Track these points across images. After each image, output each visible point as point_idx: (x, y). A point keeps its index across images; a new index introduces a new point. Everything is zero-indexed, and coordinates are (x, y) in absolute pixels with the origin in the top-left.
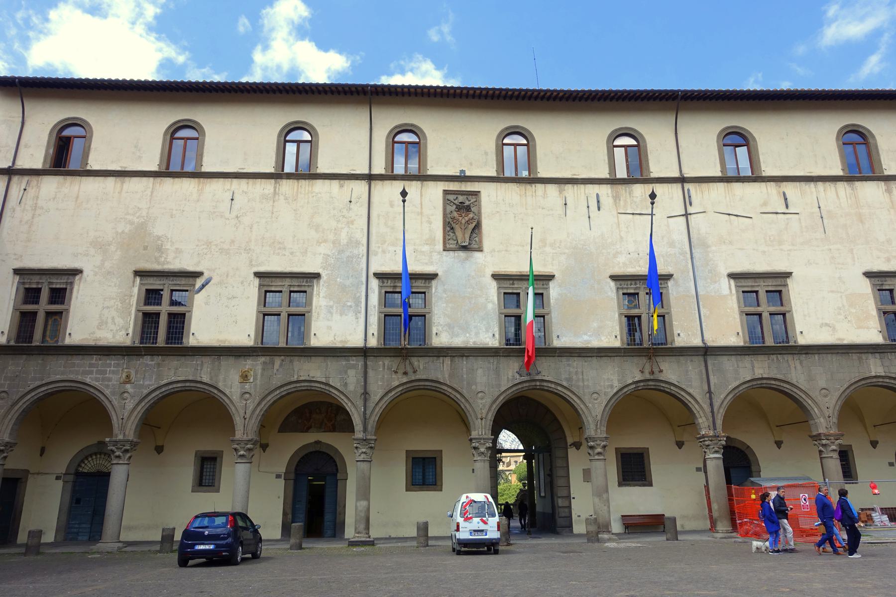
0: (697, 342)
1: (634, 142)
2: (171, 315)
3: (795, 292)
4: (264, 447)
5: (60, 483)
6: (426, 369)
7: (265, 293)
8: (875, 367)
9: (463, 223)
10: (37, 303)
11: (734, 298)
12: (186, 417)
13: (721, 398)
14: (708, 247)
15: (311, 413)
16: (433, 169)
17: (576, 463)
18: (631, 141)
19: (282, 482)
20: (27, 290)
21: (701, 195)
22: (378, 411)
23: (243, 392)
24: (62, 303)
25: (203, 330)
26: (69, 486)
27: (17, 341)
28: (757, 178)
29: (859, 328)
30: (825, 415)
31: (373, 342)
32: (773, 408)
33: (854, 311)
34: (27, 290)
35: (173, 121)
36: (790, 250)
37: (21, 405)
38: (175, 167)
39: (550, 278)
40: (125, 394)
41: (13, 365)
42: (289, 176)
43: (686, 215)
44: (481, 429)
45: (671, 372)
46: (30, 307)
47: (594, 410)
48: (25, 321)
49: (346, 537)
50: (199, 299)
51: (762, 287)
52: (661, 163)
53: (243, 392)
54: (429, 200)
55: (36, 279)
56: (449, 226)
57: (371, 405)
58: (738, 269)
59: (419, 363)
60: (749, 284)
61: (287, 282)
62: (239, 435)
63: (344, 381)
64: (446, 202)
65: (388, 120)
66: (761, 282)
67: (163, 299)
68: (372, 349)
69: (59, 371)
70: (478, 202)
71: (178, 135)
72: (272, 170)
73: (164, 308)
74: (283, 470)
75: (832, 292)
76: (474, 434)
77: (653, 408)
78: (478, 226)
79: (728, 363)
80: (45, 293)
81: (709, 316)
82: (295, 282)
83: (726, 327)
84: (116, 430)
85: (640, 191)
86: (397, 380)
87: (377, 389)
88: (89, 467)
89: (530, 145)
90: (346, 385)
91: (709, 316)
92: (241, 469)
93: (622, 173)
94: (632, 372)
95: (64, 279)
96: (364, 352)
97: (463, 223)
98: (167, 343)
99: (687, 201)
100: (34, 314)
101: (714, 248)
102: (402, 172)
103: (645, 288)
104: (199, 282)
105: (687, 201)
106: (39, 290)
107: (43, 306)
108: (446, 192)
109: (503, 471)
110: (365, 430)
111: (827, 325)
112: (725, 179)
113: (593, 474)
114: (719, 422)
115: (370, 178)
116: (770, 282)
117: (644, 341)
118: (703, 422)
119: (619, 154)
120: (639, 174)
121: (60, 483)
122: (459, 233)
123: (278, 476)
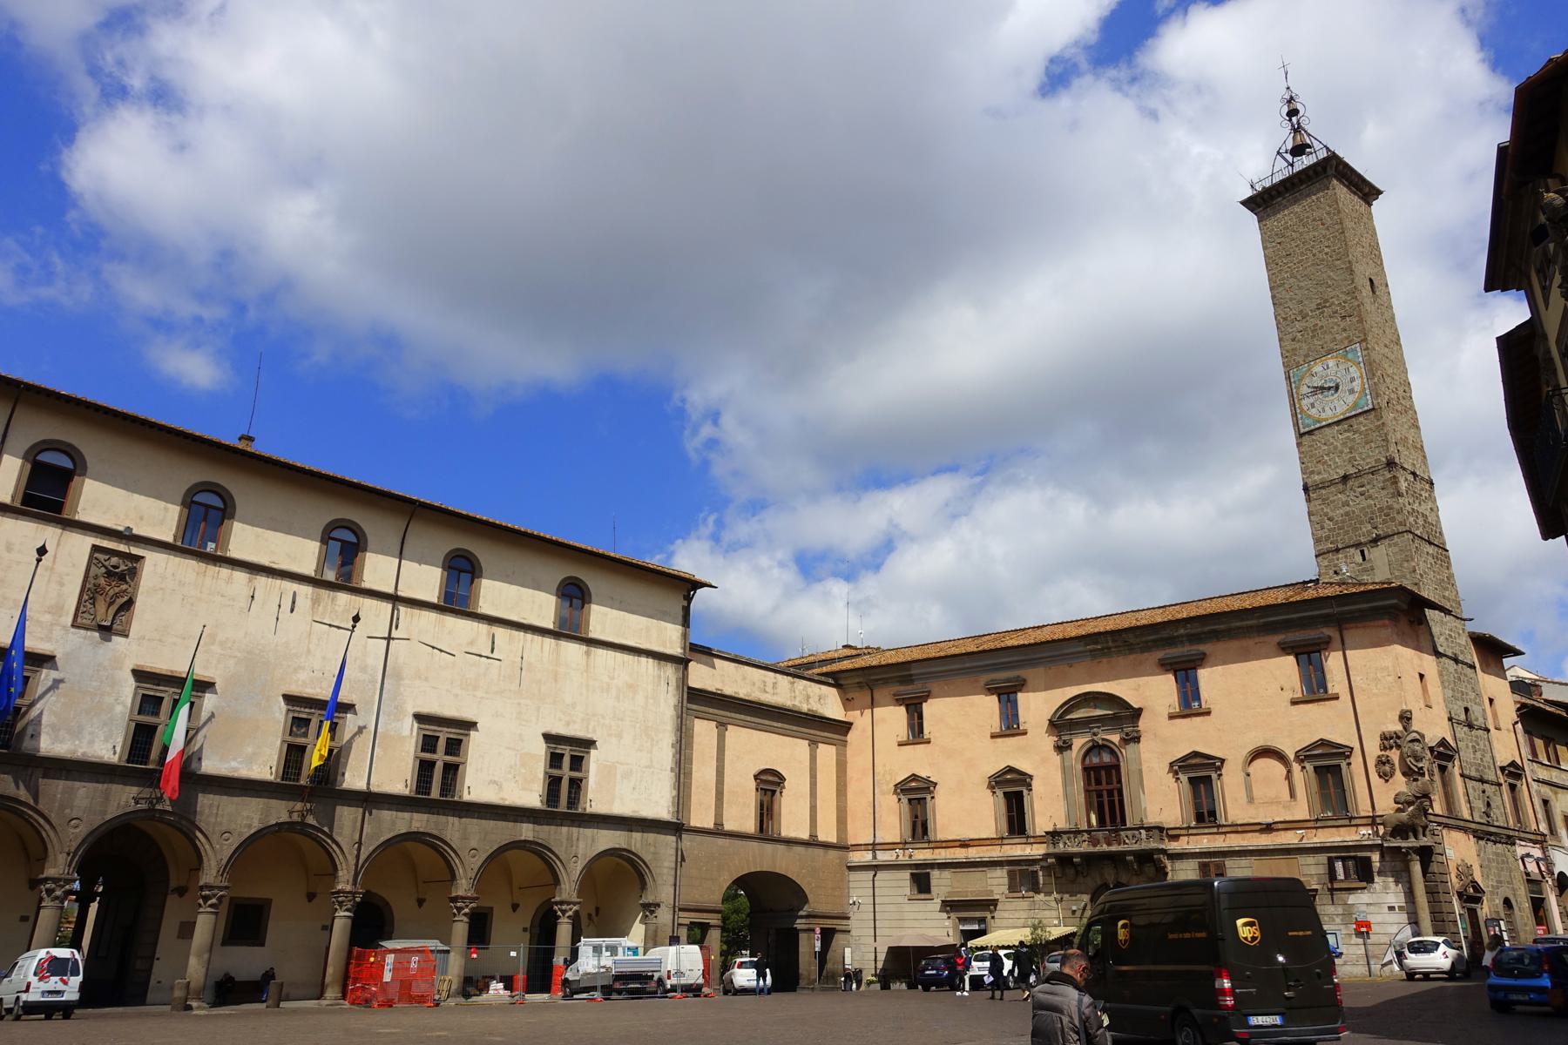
8: (527, 831)
10: (434, 752)
29: (524, 789)
43: (389, 638)
51: (444, 734)
56: (90, 593)
58: (426, 709)
83: (396, 776)
99: (394, 623)
100: (432, 764)
105: (394, 623)
111: (495, 782)
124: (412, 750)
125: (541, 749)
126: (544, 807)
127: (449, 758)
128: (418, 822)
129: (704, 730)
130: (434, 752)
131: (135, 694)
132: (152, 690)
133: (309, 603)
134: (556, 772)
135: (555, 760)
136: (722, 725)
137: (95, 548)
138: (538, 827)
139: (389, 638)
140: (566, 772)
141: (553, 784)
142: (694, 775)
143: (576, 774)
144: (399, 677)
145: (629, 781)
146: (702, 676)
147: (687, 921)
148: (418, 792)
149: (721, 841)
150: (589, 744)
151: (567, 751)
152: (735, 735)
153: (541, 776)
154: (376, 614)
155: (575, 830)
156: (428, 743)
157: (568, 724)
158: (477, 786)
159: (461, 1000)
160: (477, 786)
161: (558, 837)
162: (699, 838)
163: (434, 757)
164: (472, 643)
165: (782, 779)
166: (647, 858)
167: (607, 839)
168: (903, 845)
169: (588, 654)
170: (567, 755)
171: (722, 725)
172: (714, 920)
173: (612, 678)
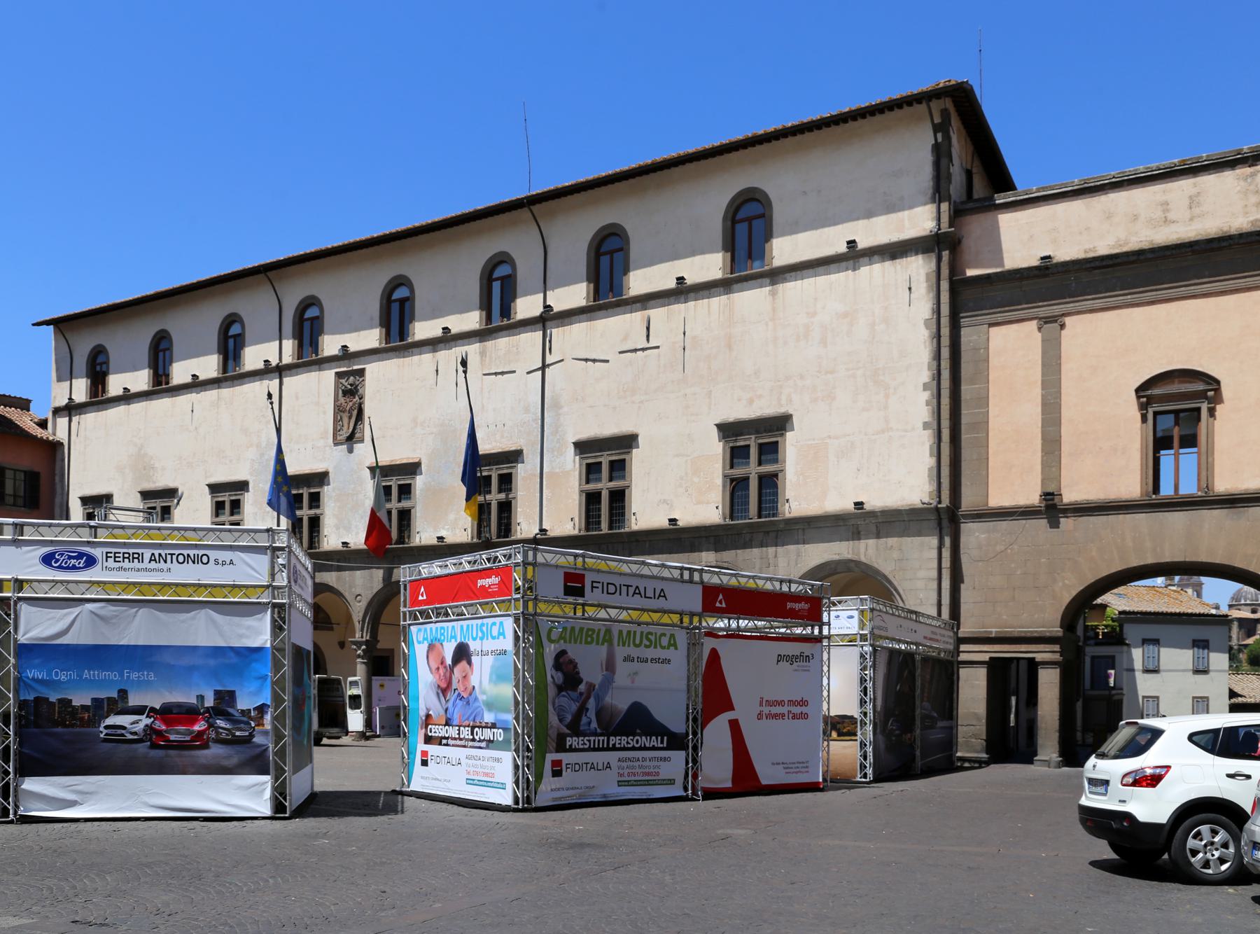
9: (350, 418)
11: (577, 473)
14: (561, 407)
21: (566, 338)
29: (699, 503)
33: (696, 480)
36: (642, 402)
39: (412, 469)
43: (544, 367)
46: (768, 468)
49: (350, 729)
51: (605, 459)
71: (740, 215)
75: (677, 456)
83: (565, 518)
97: (350, 418)
98: (732, 518)
99: (546, 347)
100: (745, 480)
101: (565, 409)
105: (546, 347)
111: (665, 501)
113: (1201, 678)
124: (577, 484)
125: (716, 449)
126: (583, 533)
127: (312, 512)
131: (581, 465)
133: (478, 357)
135: (737, 455)
136: (1053, 322)
138: (719, 554)
139: (544, 367)
141: (736, 486)
144: (557, 406)
147: (986, 657)
148: (587, 529)
150: (781, 423)
151: (752, 442)
153: (719, 481)
155: (771, 550)
156: (591, 471)
157: (751, 401)
158: (645, 513)
160: (645, 513)
163: (599, 486)
164: (625, 338)
165: (1214, 383)
168: (15, 640)
169: (773, 294)
170: (754, 444)
172: (1043, 653)
173: (814, 314)
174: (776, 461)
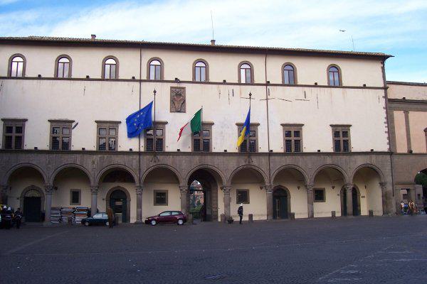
0: (267, 151)
1: (68, 61)
2: (295, 141)
3: (352, 132)
4: (56, 188)
5: (19, 201)
6: (163, 160)
7: (99, 129)
8: (329, 161)
9: (178, 100)
10: (11, 132)
12: (72, 174)
13: (274, 172)
15: (118, 175)
16: (166, 78)
17: (221, 195)
18: (248, 67)
19: (105, 201)
20: (7, 127)
22: (273, 177)
23: (93, 168)
24: (347, 137)
25: (29, 144)
26: (23, 202)
27: (6, 147)
28: (340, 86)
30: (309, 177)
31: (142, 150)
32: (291, 175)
34: (7, 127)
35: (59, 55)
37: (11, 172)
38: (60, 76)
40: (49, 169)
41: (6, 157)
42: (107, 80)
43: (267, 99)
44: (184, 183)
45: (255, 161)
46: (10, 134)
47: (226, 176)
48: (8, 140)
50: (74, 131)
52: (259, 78)
53: (93, 168)
54: (164, 92)
55: (10, 123)
56: (173, 101)
57: (142, 173)
58: (98, 120)
59: (160, 157)
60: (55, 125)
61: (108, 125)
62: (92, 184)
63: (131, 165)
64: (172, 91)
65: (148, 55)
66: (292, 128)
67: (61, 129)
68: (142, 152)
69: (23, 160)
70: (185, 91)
71: (152, 63)
72: (53, 77)
73: (293, 138)
74: (105, 197)
76: (181, 185)
77: (248, 175)
78: (184, 102)
79: (277, 158)
80: (15, 129)
81: (271, 141)
82: (111, 125)
83: (278, 146)
84: (46, 182)
85: (249, 89)
86: (152, 164)
87: (144, 168)
88: (30, 194)
89: (207, 67)
90: (132, 165)
91: (271, 141)
92: (49, 196)
93: (287, 82)
94: (242, 162)
95: (299, 127)
96: (139, 153)
99: (268, 93)
102: (109, 78)
103: (248, 128)
104: (74, 124)
105: (268, 93)
106: (290, 132)
107: (14, 134)
108: (171, 87)
109: (198, 196)
110: (140, 183)
112: (329, 87)
114: (272, 180)
115: (141, 81)
116: (295, 128)
117: (248, 147)
118: (267, 180)
119: (243, 72)
120: (251, 82)
121: (19, 201)
122: (176, 105)
123: (103, 199)
125: (330, 130)
128: (288, 161)
129: (399, 116)
130: (11, 132)
132: (55, 125)
134: (10, 134)
137: (171, 87)
139: (267, 99)
140: (341, 139)
142: (397, 133)
143: (345, 139)
145: (369, 136)
146: (396, 93)
149: (412, 158)
152: (412, 115)
154: (259, 92)
158: (76, 145)
159: (354, 217)
161: (341, 161)
162: (401, 157)
163: (293, 141)
166: (379, 166)
167: (361, 161)
170: (341, 134)
171: (406, 113)
174: (347, 137)
